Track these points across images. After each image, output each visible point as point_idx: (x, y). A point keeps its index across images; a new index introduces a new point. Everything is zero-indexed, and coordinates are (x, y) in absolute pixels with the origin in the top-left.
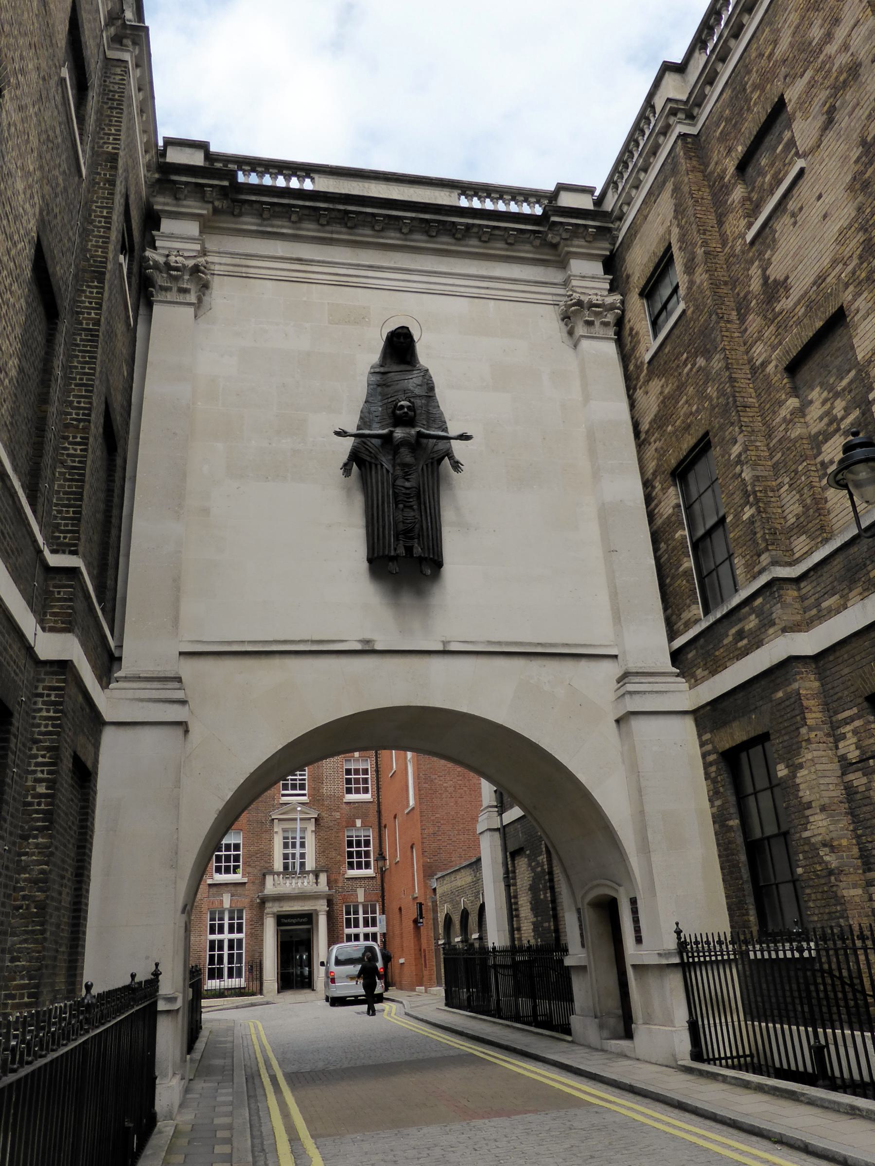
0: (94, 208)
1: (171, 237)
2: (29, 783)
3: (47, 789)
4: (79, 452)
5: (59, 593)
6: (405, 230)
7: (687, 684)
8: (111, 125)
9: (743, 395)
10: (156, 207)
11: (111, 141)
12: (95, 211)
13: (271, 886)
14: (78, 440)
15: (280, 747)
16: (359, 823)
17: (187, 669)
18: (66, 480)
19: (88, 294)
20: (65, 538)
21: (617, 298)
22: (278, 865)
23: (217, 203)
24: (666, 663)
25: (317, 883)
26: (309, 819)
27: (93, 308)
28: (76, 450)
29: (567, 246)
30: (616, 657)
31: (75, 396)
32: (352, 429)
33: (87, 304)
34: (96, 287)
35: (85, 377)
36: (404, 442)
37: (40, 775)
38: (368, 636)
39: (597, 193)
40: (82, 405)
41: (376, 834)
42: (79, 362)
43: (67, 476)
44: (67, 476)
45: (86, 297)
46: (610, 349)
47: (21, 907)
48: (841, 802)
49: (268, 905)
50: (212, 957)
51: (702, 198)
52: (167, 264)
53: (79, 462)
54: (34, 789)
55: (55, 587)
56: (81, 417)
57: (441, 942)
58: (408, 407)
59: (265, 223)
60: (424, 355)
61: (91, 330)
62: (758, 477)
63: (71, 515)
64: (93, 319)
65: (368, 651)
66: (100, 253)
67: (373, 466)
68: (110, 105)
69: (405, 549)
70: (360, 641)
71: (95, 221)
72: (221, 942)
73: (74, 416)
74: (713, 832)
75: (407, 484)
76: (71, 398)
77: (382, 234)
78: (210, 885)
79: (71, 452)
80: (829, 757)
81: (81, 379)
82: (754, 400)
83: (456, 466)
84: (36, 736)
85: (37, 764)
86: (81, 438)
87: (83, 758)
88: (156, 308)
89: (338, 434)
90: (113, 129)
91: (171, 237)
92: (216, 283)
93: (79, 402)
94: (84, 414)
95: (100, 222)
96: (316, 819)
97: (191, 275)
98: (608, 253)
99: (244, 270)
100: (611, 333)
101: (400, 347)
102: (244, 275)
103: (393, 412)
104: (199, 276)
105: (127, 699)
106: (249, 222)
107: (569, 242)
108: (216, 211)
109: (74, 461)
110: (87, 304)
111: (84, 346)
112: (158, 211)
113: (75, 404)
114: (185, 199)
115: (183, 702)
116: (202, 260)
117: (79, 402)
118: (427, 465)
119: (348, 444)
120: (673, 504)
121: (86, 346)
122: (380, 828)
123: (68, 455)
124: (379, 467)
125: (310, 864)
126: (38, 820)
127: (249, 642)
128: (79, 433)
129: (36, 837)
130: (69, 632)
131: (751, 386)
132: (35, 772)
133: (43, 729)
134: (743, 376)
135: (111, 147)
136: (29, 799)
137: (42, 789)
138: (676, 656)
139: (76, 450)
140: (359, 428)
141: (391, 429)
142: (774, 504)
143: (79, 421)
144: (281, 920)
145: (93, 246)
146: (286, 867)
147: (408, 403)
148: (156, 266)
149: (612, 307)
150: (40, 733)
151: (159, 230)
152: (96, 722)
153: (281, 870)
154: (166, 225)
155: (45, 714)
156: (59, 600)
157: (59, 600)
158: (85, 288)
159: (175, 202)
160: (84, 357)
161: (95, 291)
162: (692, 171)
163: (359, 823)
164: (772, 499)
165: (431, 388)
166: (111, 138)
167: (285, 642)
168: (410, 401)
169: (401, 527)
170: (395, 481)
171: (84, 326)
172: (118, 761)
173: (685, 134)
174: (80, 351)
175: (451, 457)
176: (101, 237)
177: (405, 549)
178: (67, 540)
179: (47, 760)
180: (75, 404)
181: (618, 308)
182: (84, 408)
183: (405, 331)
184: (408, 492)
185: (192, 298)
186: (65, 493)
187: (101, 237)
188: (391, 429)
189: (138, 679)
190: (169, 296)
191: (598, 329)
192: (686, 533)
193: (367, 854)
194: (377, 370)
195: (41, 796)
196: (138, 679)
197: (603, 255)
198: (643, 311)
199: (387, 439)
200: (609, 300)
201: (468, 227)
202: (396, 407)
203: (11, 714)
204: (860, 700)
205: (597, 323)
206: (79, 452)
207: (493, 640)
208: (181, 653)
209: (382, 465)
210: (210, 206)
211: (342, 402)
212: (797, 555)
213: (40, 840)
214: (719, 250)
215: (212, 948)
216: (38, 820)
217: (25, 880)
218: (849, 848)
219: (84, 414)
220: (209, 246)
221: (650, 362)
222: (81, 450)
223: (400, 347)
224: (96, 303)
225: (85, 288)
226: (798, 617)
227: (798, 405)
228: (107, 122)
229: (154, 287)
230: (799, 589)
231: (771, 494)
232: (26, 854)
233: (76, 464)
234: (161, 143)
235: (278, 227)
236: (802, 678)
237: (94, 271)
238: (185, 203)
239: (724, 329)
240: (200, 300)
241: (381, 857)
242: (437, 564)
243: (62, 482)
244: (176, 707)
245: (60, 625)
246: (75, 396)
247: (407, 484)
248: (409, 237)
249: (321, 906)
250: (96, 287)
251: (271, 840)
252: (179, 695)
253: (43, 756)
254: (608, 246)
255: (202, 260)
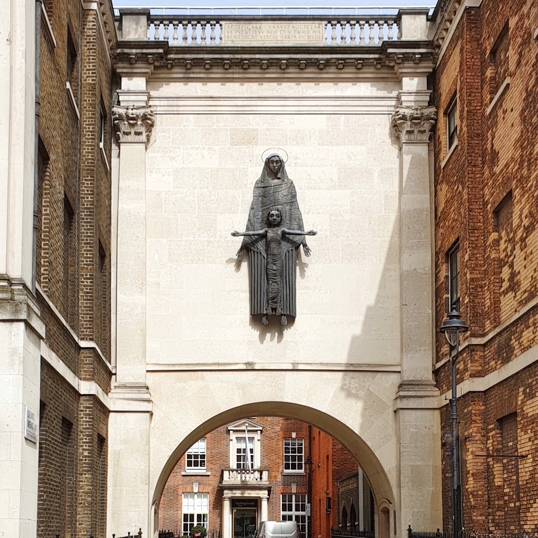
0: (85, 125)
1: (128, 92)
2: (81, 451)
3: (88, 453)
4: (89, 283)
5: (86, 360)
6: (283, 67)
7: (439, 392)
8: (90, 63)
9: (475, 220)
10: (119, 71)
11: (91, 75)
12: (86, 128)
13: (229, 479)
14: (88, 276)
15: (201, 423)
16: (294, 435)
17: (151, 380)
18: (84, 300)
19: (86, 185)
20: (86, 331)
21: (433, 109)
22: (233, 464)
23: (156, 64)
24: (429, 376)
25: (261, 478)
26: (256, 431)
27: (90, 194)
28: (87, 282)
29: (400, 68)
30: (400, 372)
31: (85, 250)
32: (242, 229)
33: (86, 192)
34: (90, 180)
35: (88, 238)
36: (273, 240)
37: (84, 447)
38: (250, 360)
39: (431, 13)
40: (89, 255)
41: (307, 444)
42: (85, 229)
43: (85, 298)
44: (85, 298)
45: (85, 187)
46: (422, 150)
47: (81, 503)
48: (483, 472)
49: (226, 492)
50: (185, 526)
51: (474, 65)
52: (127, 116)
53: (90, 289)
54: (83, 453)
55: (84, 358)
56: (88, 263)
57: (340, 525)
58: (277, 216)
59: (189, 71)
60: (288, 169)
61: (89, 208)
62: (473, 279)
63: (88, 319)
64: (89, 201)
65: (250, 368)
66: (90, 157)
67: (256, 253)
68: (88, 47)
69: (272, 311)
70: (246, 364)
71: (86, 135)
72: (297, 510)
73: (85, 262)
74: (441, 478)
75: (275, 268)
76: (83, 252)
77: (267, 71)
78: (183, 476)
79: (86, 283)
80: (481, 448)
81: (87, 240)
82: (481, 225)
83: (307, 251)
84: (82, 430)
85: (83, 443)
86: (90, 275)
87: (101, 434)
88: (122, 146)
89: (234, 235)
90: (91, 65)
91: (128, 92)
92: (158, 120)
93: (87, 254)
94: (90, 261)
95: (89, 135)
96: (261, 431)
97: (142, 120)
98: (431, 70)
99: (175, 108)
100: (425, 137)
101: (274, 168)
102: (176, 112)
103: (268, 219)
104: (148, 121)
105: (120, 399)
106: (178, 72)
107: (401, 65)
108: (156, 68)
109: (87, 289)
110: (86, 192)
111: (87, 219)
112: (119, 73)
113: (85, 255)
114: (136, 63)
115: (149, 401)
116: (148, 110)
117: (87, 254)
118: (288, 252)
119: (240, 240)
120: (444, 275)
121: (87, 219)
122: (311, 439)
123: (84, 286)
124: (259, 254)
125: (257, 464)
126: (85, 467)
127: (196, 364)
128: (88, 272)
129: (85, 474)
130: (93, 380)
131: (481, 214)
132: (82, 446)
133: (84, 427)
134: (477, 207)
135: (91, 79)
136: (81, 458)
137: (86, 453)
138: (436, 372)
139: (87, 282)
140: (248, 229)
141: (266, 229)
142: (480, 297)
143: (88, 265)
144: (234, 502)
145: (86, 152)
146: (239, 466)
147: (277, 212)
148: (120, 118)
149: (428, 118)
150: (83, 428)
151: (120, 89)
152: (105, 411)
153: (235, 467)
154: (125, 82)
155: (84, 419)
156: (87, 364)
157: (87, 364)
158: (84, 181)
159: (129, 66)
160: (87, 226)
161: (89, 182)
162: (470, 42)
163: (294, 435)
164: (479, 293)
165: (294, 196)
166: (91, 72)
167: (204, 364)
168: (278, 210)
169: (271, 296)
170: (267, 265)
171: (86, 206)
172: (117, 429)
173: (470, 7)
174: (85, 222)
175: (305, 245)
176: (90, 146)
177: (272, 311)
178: (88, 333)
179: (87, 441)
180: (85, 255)
181: (432, 119)
182: (90, 258)
183: (277, 159)
184: (275, 272)
185: (143, 138)
186: (85, 307)
187: (90, 146)
188: (266, 229)
189: (125, 387)
190: (129, 138)
191: (419, 137)
192: (449, 296)
193: (300, 458)
194: (259, 185)
195: (86, 456)
196: (125, 387)
197: (428, 72)
198: (444, 127)
199: (264, 236)
200: (427, 112)
201: (328, 60)
202: (269, 215)
203: (72, 424)
204: (495, 421)
205: (133, 133)
206: (89, 283)
207: (324, 362)
208: (147, 371)
209: (261, 253)
210: (152, 67)
211: (237, 217)
212: (486, 331)
213: (87, 476)
214: (479, 108)
215: (186, 519)
216: (85, 467)
217: (82, 492)
218: (482, 496)
219: (90, 261)
220: (153, 93)
221: (443, 169)
222: (90, 282)
223: (274, 168)
224: (91, 191)
225: (84, 181)
226: (480, 368)
227: (497, 237)
228: (87, 61)
229: (120, 131)
230: (484, 352)
231: (479, 290)
232: (82, 481)
233: (88, 291)
234: (117, 13)
235: (197, 73)
236: (474, 404)
237: (88, 170)
238: (136, 65)
239: (470, 172)
240: (148, 137)
241: (309, 461)
242: (291, 319)
243: (82, 301)
244: (146, 404)
245: (88, 377)
246: (85, 250)
247: (275, 268)
248: (286, 71)
249: (264, 494)
250: (90, 180)
251: (228, 445)
252: (147, 396)
253: (86, 439)
254: (431, 65)
255: (148, 110)
